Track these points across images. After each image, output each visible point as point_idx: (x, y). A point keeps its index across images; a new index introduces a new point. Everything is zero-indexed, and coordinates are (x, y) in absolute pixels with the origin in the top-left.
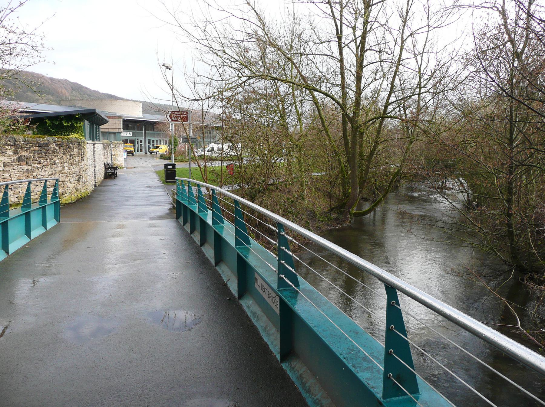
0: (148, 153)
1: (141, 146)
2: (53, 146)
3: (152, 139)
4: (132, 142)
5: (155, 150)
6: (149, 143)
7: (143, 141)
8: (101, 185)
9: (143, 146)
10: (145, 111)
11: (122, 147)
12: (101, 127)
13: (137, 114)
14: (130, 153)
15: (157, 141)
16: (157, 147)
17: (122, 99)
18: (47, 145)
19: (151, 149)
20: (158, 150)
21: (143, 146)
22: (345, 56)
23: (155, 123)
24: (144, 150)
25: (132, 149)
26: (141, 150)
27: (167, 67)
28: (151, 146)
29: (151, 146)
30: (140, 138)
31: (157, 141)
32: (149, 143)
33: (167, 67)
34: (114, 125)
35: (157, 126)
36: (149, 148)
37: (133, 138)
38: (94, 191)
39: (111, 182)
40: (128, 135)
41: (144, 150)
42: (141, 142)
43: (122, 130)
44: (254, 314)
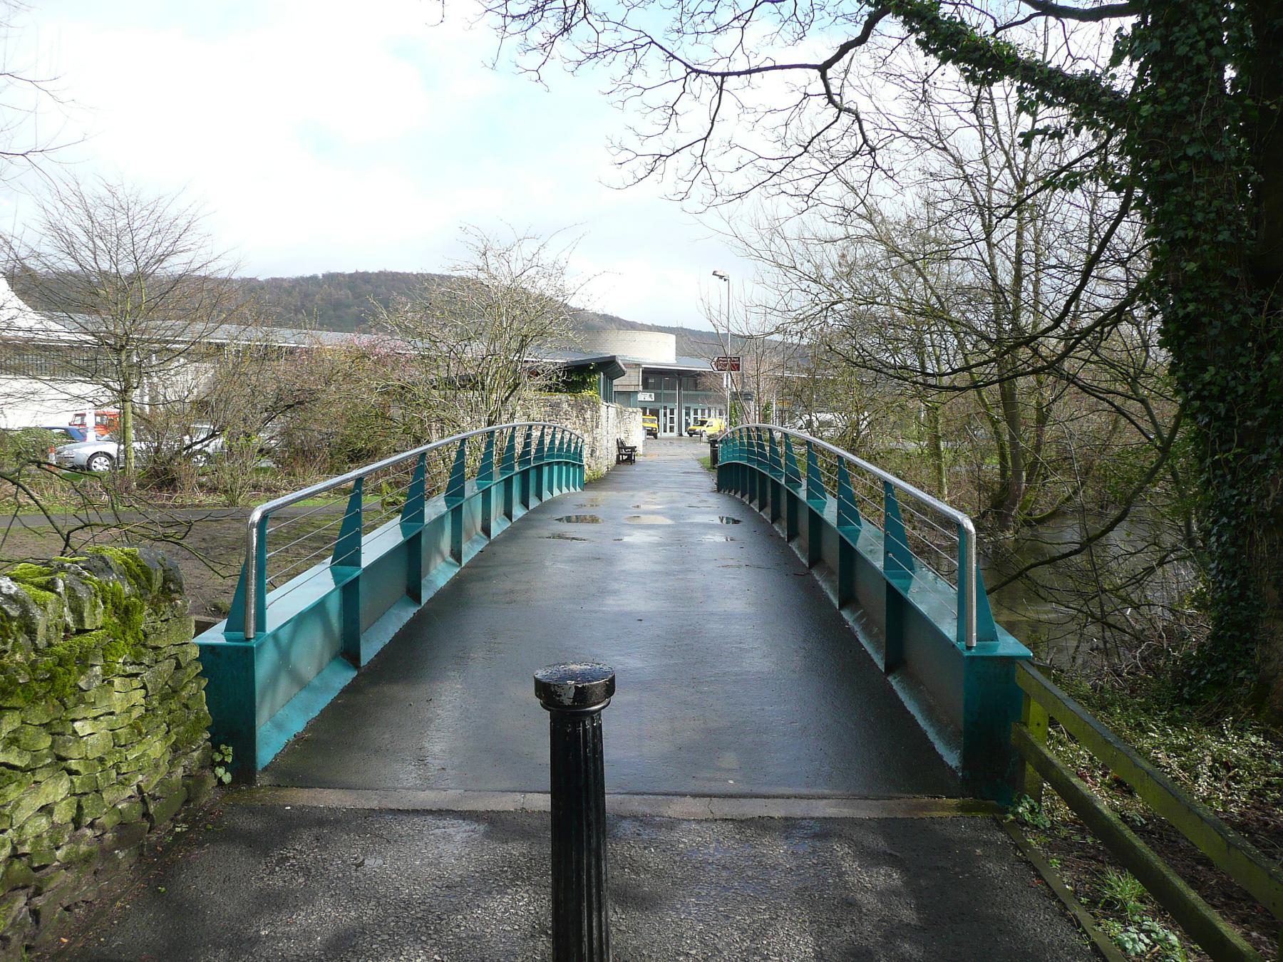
0: (685, 434)
1: (672, 420)
2: (565, 406)
3: (693, 406)
4: (655, 413)
5: (698, 429)
6: (688, 414)
7: (676, 412)
8: (614, 469)
9: (676, 420)
10: (680, 352)
11: (640, 416)
12: (615, 382)
13: (663, 353)
14: (652, 433)
15: (703, 410)
16: (703, 423)
17: (632, 326)
18: (558, 404)
19: (691, 427)
20: (703, 428)
21: (676, 416)
22: (998, 262)
23: (699, 374)
24: (676, 429)
25: (655, 426)
26: (672, 429)
27: (721, 277)
28: (691, 421)
29: (691, 421)
30: (670, 406)
31: (703, 410)
32: (688, 414)
33: (721, 277)
34: (631, 380)
35: (703, 379)
36: (688, 424)
37: (657, 405)
38: (608, 473)
39: (625, 468)
40: (648, 399)
41: (676, 429)
42: (672, 413)
43: (641, 388)
44: (924, 808)
